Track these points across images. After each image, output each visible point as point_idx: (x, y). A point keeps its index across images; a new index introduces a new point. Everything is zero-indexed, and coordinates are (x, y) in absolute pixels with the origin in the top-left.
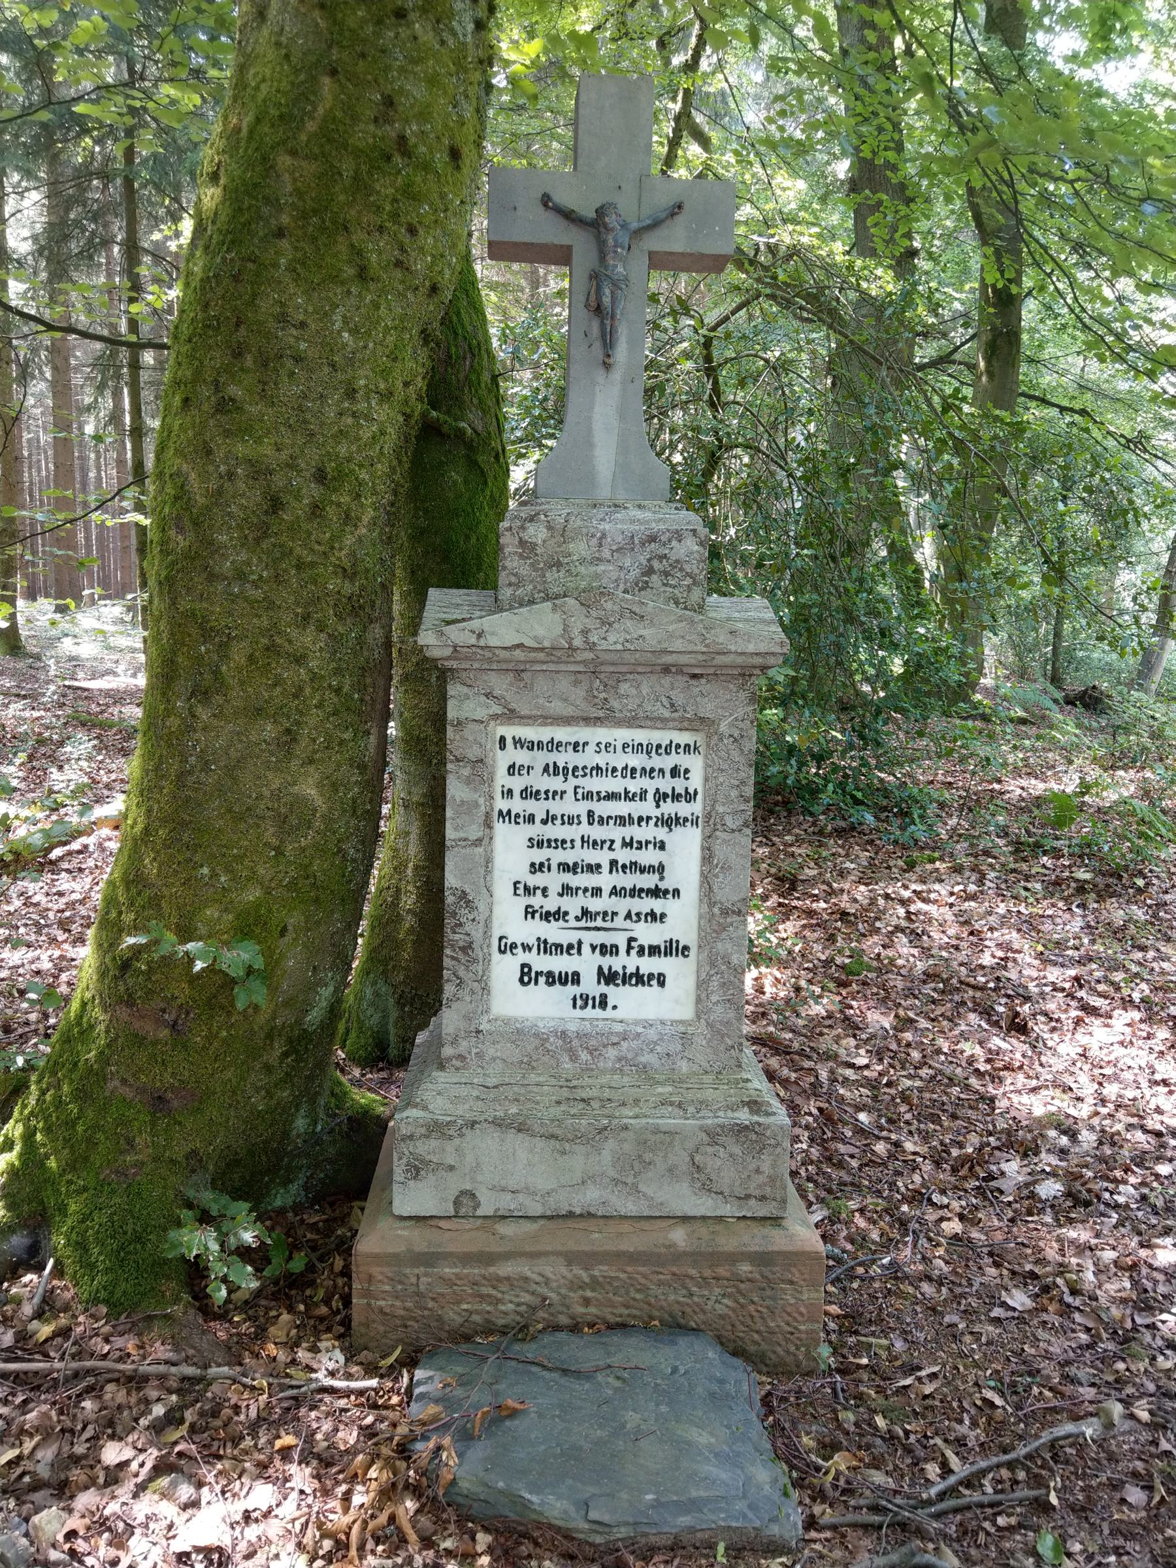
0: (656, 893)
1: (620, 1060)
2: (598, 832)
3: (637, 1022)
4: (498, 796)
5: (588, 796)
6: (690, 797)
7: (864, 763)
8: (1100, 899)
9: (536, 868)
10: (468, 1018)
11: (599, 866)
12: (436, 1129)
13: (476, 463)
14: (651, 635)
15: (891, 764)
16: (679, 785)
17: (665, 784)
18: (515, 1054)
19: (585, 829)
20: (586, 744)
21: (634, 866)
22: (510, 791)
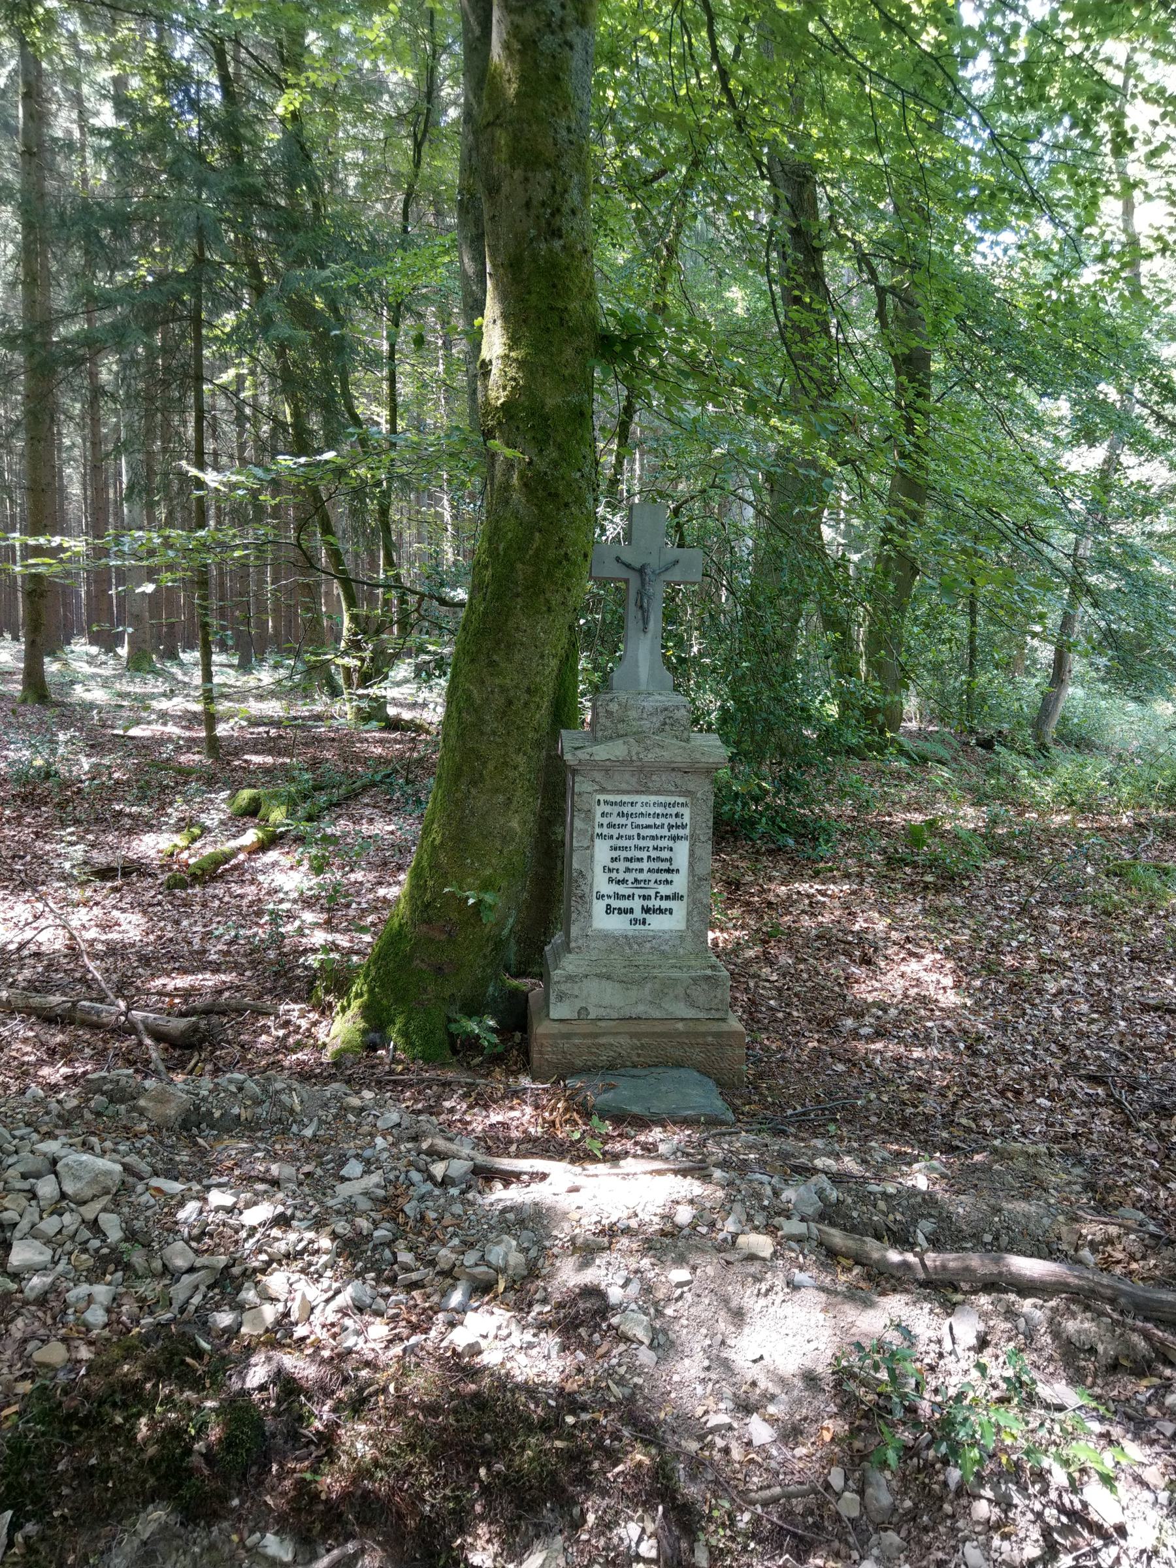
0: (668, 871)
2: (642, 843)
6: (684, 827)
7: (789, 802)
8: (937, 892)
9: (614, 860)
12: (570, 978)
14: (666, 754)
15: (808, 801)
17: (673, 821)
21: (659, 859)
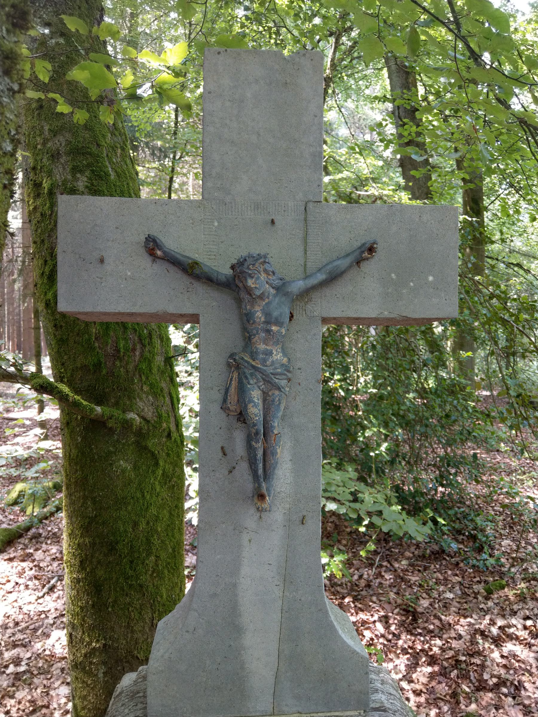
13: (146, 448)
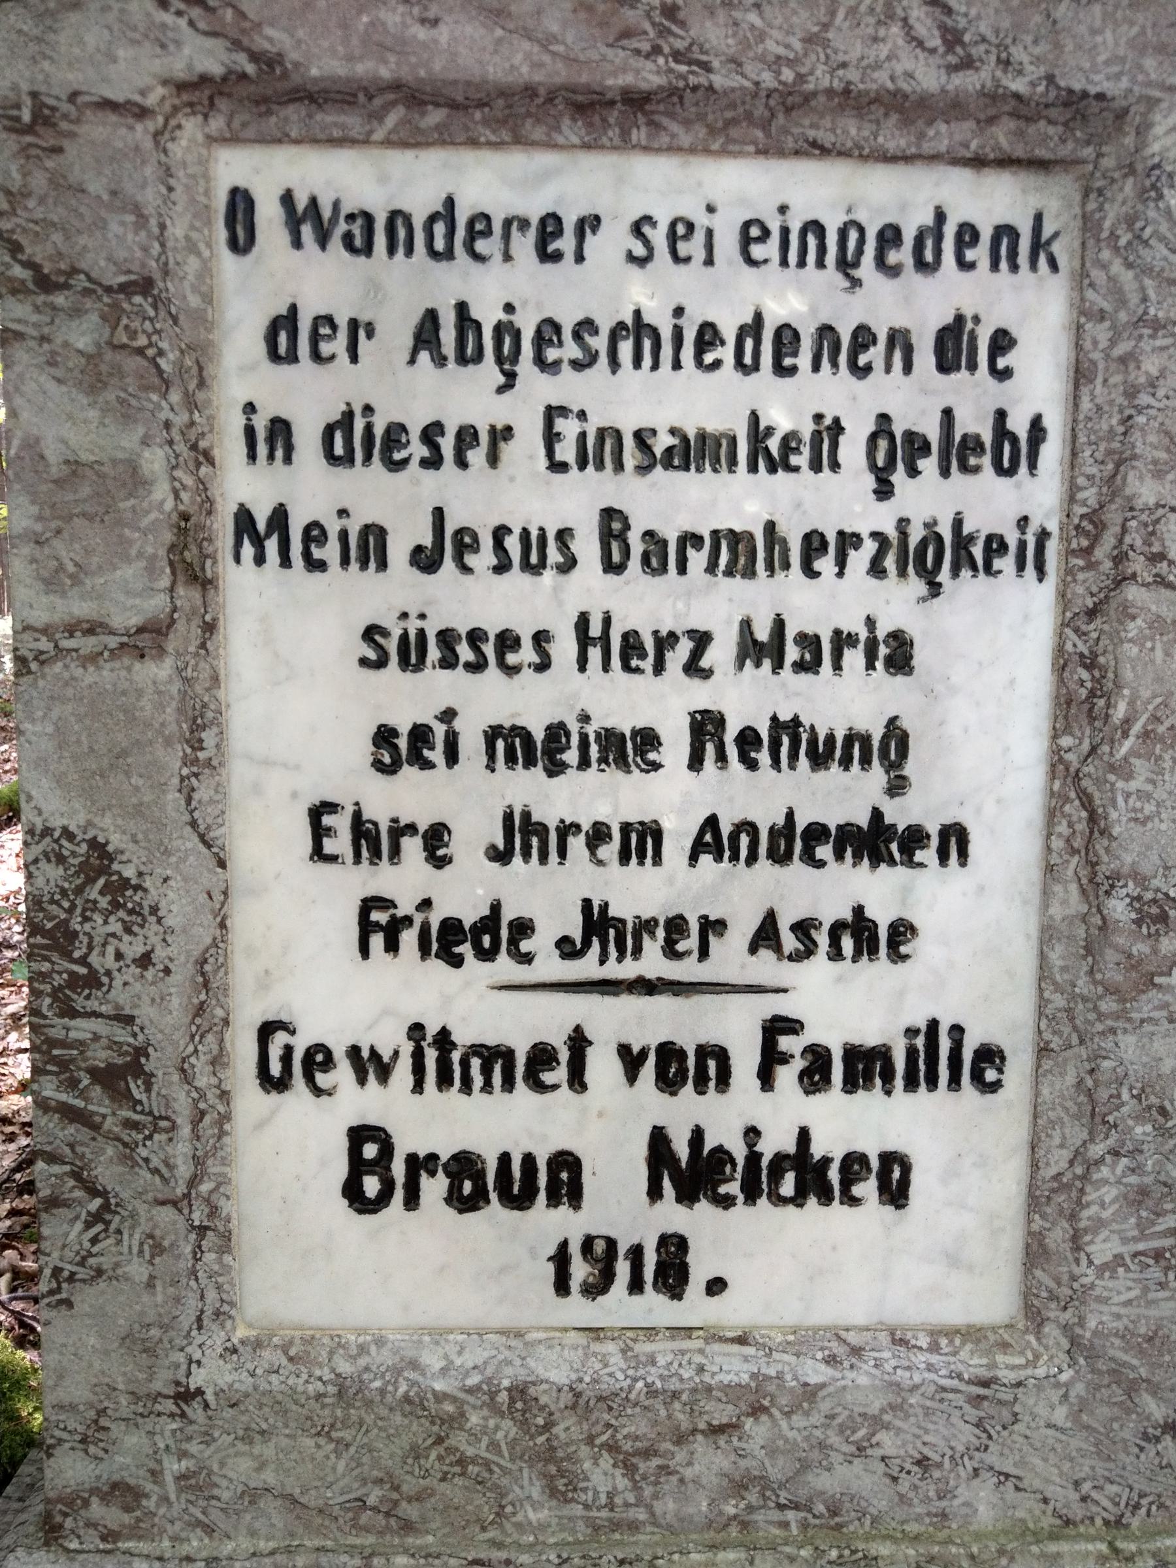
0: (873, 842)
1: (739, 1487)
3: (801, 1340)
4: (231, 448)
5: (602, 450)
6: (1011, 450)
10: (141, 1344)
11: (648, 739)
16: (972, 400)
17: (914, 398)
18: (332, 1476)
19: (588, 588)
20: (589, 224)
22: (281, 430)
